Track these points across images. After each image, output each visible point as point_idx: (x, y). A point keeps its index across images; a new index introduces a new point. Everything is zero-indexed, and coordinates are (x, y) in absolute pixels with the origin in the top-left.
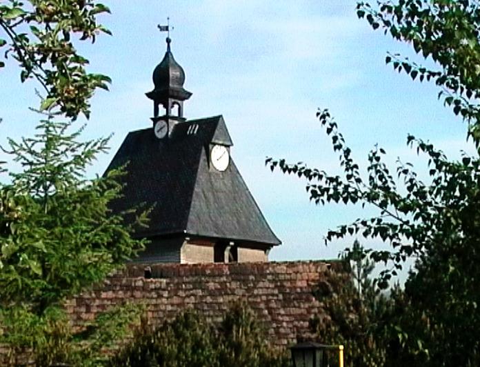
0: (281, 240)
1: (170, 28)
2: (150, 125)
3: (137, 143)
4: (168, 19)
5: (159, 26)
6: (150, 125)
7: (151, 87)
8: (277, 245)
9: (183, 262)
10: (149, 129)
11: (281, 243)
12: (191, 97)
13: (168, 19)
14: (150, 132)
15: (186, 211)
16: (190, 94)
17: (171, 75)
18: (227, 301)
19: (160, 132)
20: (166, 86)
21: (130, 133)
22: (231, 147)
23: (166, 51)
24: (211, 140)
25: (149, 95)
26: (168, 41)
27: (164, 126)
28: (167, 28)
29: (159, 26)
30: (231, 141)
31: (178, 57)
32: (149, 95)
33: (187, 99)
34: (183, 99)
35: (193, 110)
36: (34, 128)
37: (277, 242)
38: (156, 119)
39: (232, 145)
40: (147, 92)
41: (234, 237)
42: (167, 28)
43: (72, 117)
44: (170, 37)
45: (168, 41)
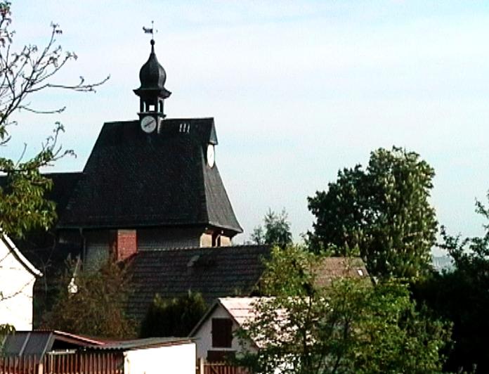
0: (243, 228)
1: (154, 31)
2: (137, 118)
3: (113, 134)
4: (153, 22)
5: (144, 28)
6: (137, 118)
7: (138, 85)
8: (240, 233)
9: (201, 246)
10: (136, 121)
11: (242, 230)
12: (171, 96)
13: (153, 22)
14: (136, 124)
15: (203, 204)
16: (170, 93)
17: (160, 76)
18: (131, 279)
19: (147, 127)
20: (151, 84)
21: (106, 124)
22: (216, 146)
23: (150, 52)
24: (209, 139)
25: (136, 92)
26: (152, 42)
27: (152, 122)
28: (151, 31)
29: (144, 28)
30: (216, 140)
31: (160, 59)
32: (136, 92)
33: (168, 97)
34: (165, 97)
35: (173, 109)
36: (55, 122)
37: (240, 231)
38: (142, 116)
39: (217, 144)
40: (135, 89)
41: (226, 227)
42: (151, 31)
43: (359, 169)
44: (155, 40)
45: (152, 42)
